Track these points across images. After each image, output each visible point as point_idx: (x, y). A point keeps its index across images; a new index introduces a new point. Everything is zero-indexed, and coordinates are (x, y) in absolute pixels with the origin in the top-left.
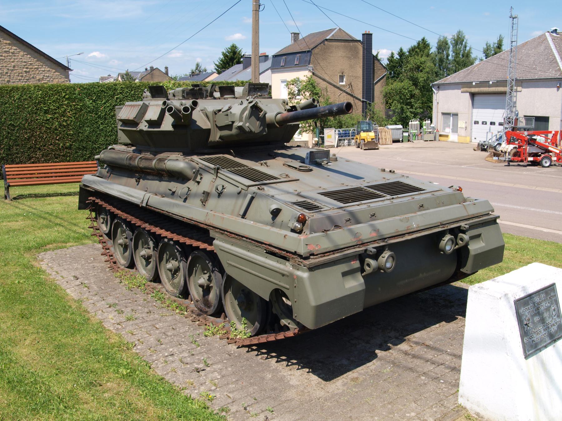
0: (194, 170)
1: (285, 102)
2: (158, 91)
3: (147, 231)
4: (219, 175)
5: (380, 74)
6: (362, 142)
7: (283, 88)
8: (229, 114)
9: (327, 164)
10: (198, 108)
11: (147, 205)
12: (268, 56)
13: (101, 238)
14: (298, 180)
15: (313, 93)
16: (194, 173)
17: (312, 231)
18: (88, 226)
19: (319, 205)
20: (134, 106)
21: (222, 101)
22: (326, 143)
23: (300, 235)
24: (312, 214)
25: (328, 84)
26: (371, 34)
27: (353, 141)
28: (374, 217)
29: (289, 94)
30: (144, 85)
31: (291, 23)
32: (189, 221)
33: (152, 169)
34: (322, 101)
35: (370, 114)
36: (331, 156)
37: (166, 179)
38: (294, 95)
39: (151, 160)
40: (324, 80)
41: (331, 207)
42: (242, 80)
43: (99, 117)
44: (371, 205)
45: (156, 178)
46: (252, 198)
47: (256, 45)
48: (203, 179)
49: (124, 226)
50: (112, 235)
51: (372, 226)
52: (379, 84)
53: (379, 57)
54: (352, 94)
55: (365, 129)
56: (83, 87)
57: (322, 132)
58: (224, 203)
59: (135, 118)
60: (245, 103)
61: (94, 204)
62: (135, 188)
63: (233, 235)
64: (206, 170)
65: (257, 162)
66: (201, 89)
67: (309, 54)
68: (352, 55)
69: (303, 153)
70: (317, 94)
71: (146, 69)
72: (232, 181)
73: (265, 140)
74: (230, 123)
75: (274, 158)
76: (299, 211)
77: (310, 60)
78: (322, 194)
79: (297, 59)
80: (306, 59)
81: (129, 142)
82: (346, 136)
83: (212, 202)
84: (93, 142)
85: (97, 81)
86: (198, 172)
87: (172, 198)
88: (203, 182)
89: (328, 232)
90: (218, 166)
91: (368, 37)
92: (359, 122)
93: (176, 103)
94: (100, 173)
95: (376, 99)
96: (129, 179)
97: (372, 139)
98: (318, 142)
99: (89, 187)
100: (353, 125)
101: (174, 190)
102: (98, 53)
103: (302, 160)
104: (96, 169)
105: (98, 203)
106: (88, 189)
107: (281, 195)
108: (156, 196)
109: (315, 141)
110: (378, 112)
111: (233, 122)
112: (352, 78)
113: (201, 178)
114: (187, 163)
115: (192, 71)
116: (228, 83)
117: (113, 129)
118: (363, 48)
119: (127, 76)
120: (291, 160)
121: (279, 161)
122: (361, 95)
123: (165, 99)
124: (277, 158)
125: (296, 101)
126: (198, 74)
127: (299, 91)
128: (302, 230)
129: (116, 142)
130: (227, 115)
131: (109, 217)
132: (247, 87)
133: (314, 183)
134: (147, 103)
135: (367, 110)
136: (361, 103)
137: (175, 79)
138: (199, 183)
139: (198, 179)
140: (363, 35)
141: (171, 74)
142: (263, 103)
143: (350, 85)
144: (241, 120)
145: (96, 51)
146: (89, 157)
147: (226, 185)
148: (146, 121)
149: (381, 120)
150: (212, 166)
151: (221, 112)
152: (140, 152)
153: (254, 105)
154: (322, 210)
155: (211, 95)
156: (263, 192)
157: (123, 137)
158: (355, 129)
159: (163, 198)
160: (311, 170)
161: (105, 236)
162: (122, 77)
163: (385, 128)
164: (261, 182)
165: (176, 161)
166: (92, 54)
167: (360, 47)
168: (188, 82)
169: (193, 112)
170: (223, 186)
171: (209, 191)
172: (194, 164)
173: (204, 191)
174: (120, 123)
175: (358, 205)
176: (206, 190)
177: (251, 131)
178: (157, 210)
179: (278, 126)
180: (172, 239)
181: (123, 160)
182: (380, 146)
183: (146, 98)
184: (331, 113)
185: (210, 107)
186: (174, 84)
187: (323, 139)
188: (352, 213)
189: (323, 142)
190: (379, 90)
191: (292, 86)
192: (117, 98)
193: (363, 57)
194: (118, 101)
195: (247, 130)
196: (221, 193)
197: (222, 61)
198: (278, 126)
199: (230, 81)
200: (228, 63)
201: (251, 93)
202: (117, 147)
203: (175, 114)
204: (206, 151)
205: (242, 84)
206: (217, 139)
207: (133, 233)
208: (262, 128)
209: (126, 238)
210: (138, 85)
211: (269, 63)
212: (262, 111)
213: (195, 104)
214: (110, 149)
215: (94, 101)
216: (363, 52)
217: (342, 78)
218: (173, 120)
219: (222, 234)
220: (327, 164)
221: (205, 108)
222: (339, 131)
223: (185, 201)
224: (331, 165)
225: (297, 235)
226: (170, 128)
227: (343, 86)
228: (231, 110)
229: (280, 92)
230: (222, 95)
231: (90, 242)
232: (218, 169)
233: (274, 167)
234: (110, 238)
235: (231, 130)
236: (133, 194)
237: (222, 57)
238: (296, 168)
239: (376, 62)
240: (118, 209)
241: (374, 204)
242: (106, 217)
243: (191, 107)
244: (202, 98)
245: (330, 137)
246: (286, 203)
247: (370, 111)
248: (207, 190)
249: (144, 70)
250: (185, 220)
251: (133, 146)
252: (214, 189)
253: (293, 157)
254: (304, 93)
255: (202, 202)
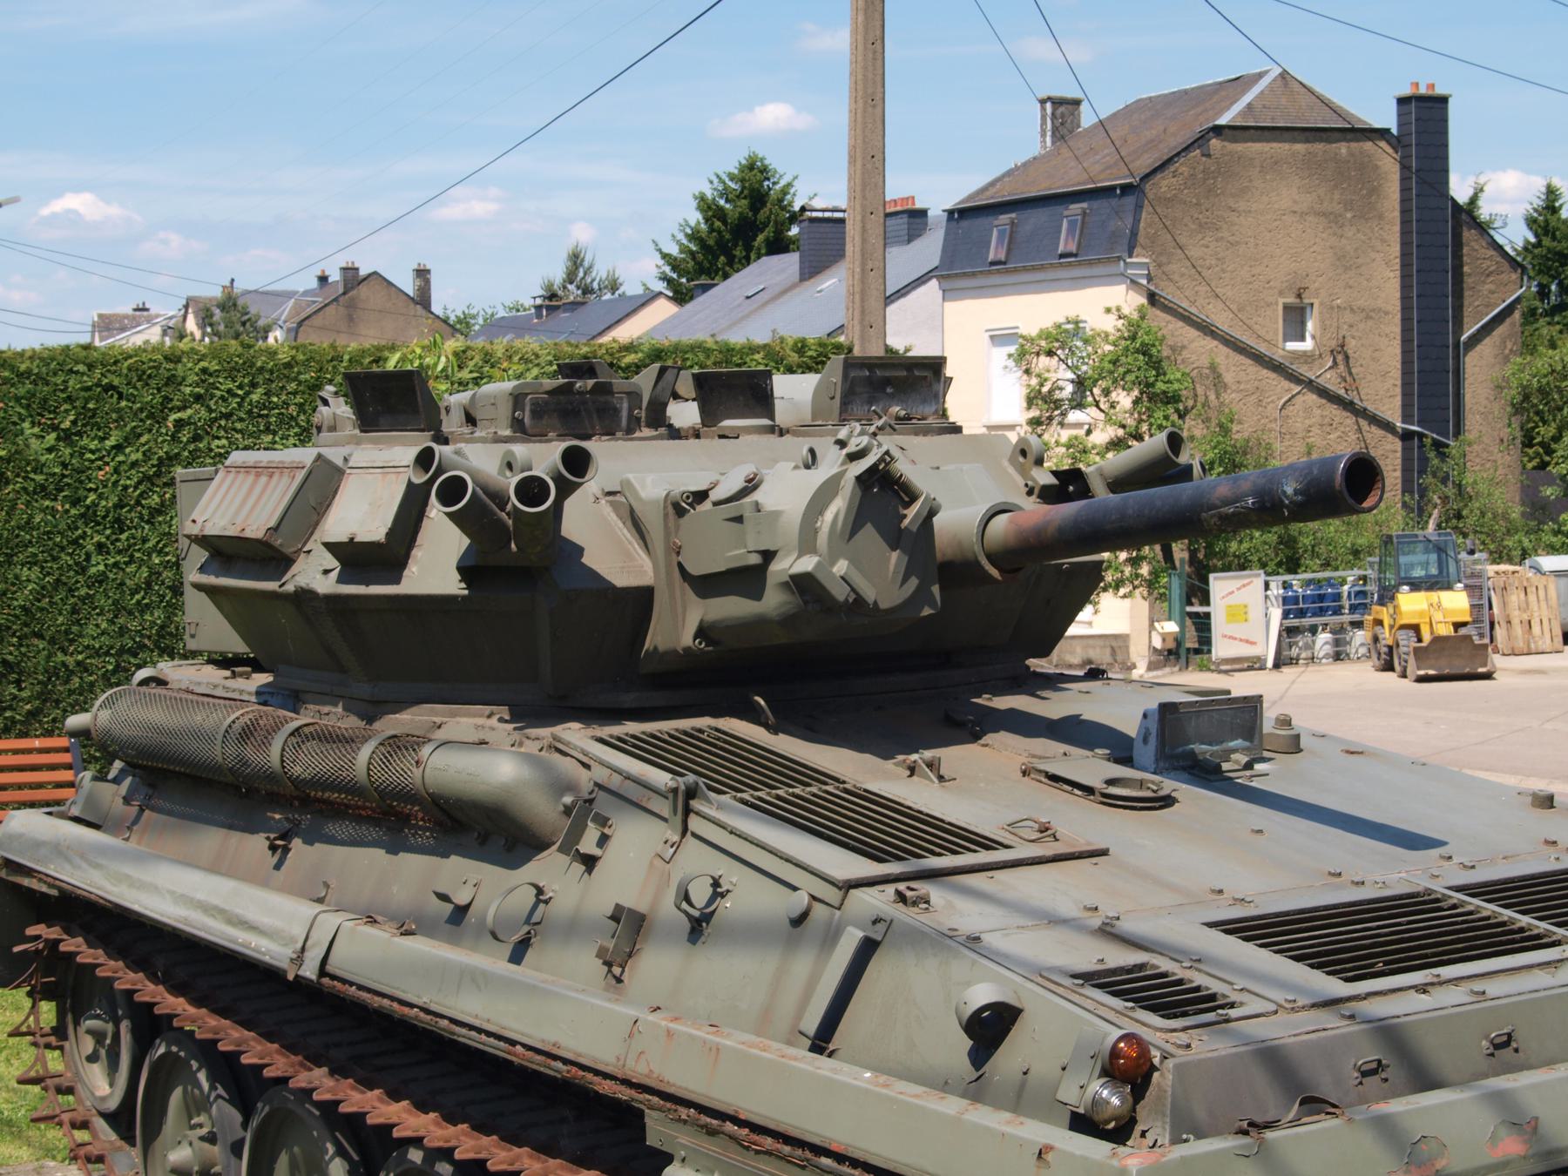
0: (568, 799)
1: (1026, 455)
2: (390, 399)
3: (320, 1105)
4: (695, 823)
5: (1490, 293)
6: (1407, 642)
7: (1002, 370)
8: (747, 515)
9: (1249, 766)
10: (592, 485)
11: (323, 972)
12: (923, 213)
13: (82, 1136)
14: (1103, 853)
15: (1155, 397)
16: (568, 811)
17: (1185, 1127)
18: (17, 1069)
19: (1215, 987)
20: (270, 470)
21: (711, 445)
22: (1221, 648)
23: (1121, 1149)
24: (1183, 1038)
25: (1224, 350)
26: (1444, 100)
27: (1360, 637)
28: (1506, 1053)
29: (1030, 401)
30: (323, 364)
31: (1038, 49)
32: (536, 1063)
33: (352, 788)
34: (1197, 433)
35: (1445, 499)
36: (1268, 726)
37: (425, 838)
38: (1057, 404)
39: (349, 741)
40: (1207, 329)
41: (1279, 996)
42: (798, 334)
43: (89, 516)
44: (1493, 988)
45: (373, 833)
46: (868, 949)
47: (869, 158)
48: (613, 845)
49: (202, 1076)
50: (135, 1120)
51: (1500, 1099)
52: (1487, 347)
53: (1484, 211)
54: (1352, 396)
55: (1418, 573)
56: (13, 368)
57: (1198, 591)
58: (723, 971)
59: (276, 529)
60: (831, 461)
61: (53, 958)
62: (265, 883)
63: (768, 1142)
64: (631, 799)
65: (887, 756)
66: (604, 389)
67: (1130, 201)
68: (1349, 205)
69: (1121, 709)
70: (1171, 399)
71: (323, 279)
72: (766, 860)
73: (933, 644)
74: (755, 559)
75: (975, 737)
76: (1111, 1022)
77: (1134, 234)
78: (1232, 928)
79: (1072, 224)
80: (1114, 224)
81: (236, 644)
82: (1321, 612)
83: (656, 964)
84: (52, 641)
85: (85, 339)
86: (587, 809)
87: (454, 941)
88: (611, 859)
89: (1269, 1135)
90: (691, 778)
91: (1426, 115)
92: (1388, 540)
93: (482, 459)
94: (91, 802)
95: (1474, 422)
96: (236, 837)
97: (1458, 626)
98: (1179, 641)
99: (29, 872)
100: (1356, 553)
101: (461, 898)
102: (88, 197)
103: (1120, 749)
104: (67, 775)
105: (71, 956)
106: (26, 882)
107: (1017, 932)
108: (368, 929)
109: (1164, 638)
110: (1482, 487)
111: (768, 556)
112: (1348, 317)
113: (603, 840)
114: (528, 758)
115: (549, 287)
116: (728, 351)
117: (154, 573)
118: (1405, 167)
119: (231, 314)
120: (1062, 747)
121: (1002, 753)
122: (1398, 401)
123: (423, 440)
124: (990, 738)
125: (1065, 435)
126: (575, 305)
127: (1081, 384)
128: (1132, 1121)
129: (169, 643)
130: (739, 519)
131: (125, 1026)
132: (837, 378)
133: (1188, 871)
134: (335, 455)
135: (1429, 479)
136: (1398, 444)
137: (460, 326)
138: (590, 862)
139: (588, 845)
140: (1402, 101)
141: (445, 301)
142: (915, 459)
143: (1341, 354)
144: (807, 544)
145: (78, 188)
146: (32, 714)
147: (732, 875)
148: (328, 545)
149: (1500, 527)
150: (662, 778)
151: (707, 506)
152: (294, 700)
153: (873, 469)
154: (1233, 1013)
155: (658, 418)
156: (924, 918)
157: (208, 625)
158: (1371, 573)
159: (408, 942)
160: (1167, 801)
161: (100, 1124)
162: (206, 319)
163: (1524, 571)
164: (912, 865)
165: (477, 752)
166: (58, 206)
167: (1387, 163)
168: (530, 343)
169: (569, 504)
170: (716, 884)
171: (642, 906)
172: (567, 766)
173: (619, 908)
174: (199, 555)
175: (1423, 989)
176: (628, 903)
177: (859, 601)
178: (377, 1001)
179: (994, 572)
180: (446, 1154)
181: (209, 738)
182: (1497, 661)
183: (333, 429)
184: (1269, 509)
185: (649, 479)
186: (461, 357)
187: (1203, 624)
188: (1389, 1033)
189: (1205, 641)
190: (1487, 376)
191: (1044, 361)
192: (180, 424)
193: (1405, 212)
194: (185, 436)
195: (840, 593)
196: (707, 917)
197: (694, 236)
198: (994, 572)
199: (737, 338)
200: (723, 248)
201: (858, 409)
202: (177, 672)
203: (478, 514)
204: (629, 700)
205: (808, 358)
206: (687, 639)
207: (247, 1116)
208: (913, 582)
209: (211, 1139)
210: (283, 357)
211: (929, 249)
212: (913, 498)
213: (577, 462)
214: (145, 682)
215: (66, 437)
216: (1405, 190)
217: (1295, 318)
218: (466, 541)
219: (712, 1132)
220: (1249, 766)
221: (627, 483)
222: (1286, 586)
223: (517, 957)
224: (1272, 775)
225: (1104, 1147)
226: (452, 585)
227: (1304, 357)
228: (757, 496)
229: (987, 396)
230: (710, 416)
231: (25, 1153)
232: (691, 793)
233: (973, 784)
234: (129, 1138)
235: (756, 593)
236: (252, 915)
237: (695, 217)
238: (1089, 790)
239: (1468, 235)
240: (177, 989)
241: (1508, 982)
242: (110, 1027)
243: (558, 479)
244: (610, 432)
245: (1238, 613)
246: (1043, 975)
247: (1444, 481)
248: (633, 900)
249: (314, 284)
250: (518, 1056)
251: (258, 667)
252: (670, 896)
253: (1074, 731)
254: (1106, 392)
255: (609, 964)
